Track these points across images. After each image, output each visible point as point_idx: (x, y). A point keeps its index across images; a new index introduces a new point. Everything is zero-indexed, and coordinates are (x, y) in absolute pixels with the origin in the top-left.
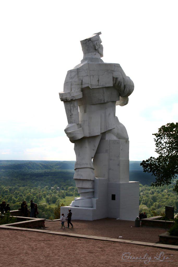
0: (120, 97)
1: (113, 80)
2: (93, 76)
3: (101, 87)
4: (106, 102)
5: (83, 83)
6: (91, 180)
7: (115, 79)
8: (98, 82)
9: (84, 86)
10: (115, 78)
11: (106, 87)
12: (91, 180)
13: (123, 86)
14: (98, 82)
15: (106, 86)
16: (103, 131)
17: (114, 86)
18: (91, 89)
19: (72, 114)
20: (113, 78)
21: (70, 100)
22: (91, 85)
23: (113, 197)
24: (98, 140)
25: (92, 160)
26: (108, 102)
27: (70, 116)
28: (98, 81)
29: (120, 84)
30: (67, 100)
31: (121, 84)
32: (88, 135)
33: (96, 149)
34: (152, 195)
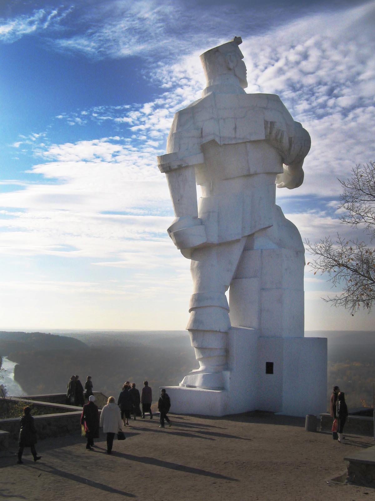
0: (283, 164)
1: (265, 128)
2: (224, 119)
3: (240, 141)
4: (252, 171)
5: (204, 135)
6: (220, 332)
7: (269, 125)
8: (235, 132)
9: (205, 140)
10: (269, 123)
11: (250, 142)
12: (221, 332)
13: (287, 141)
14: (235, 132)
15: (252, 139)
16: (247, 234)
17: (267, 140)
18: (221, 146)
19: (182, 197)
20: (266, 122)
21: (176, 167)
22: (220, 138)
23: (270, 368)
24: (237, 252)
25: (227, 293)
26: (256, 174)
27: (179, 201)
28: (235, 129)
29: (279, 137)
30: (169, 167)
31: (282, 135)
32: (214, 239)
33: (234, 268)
34: (111, 44)
